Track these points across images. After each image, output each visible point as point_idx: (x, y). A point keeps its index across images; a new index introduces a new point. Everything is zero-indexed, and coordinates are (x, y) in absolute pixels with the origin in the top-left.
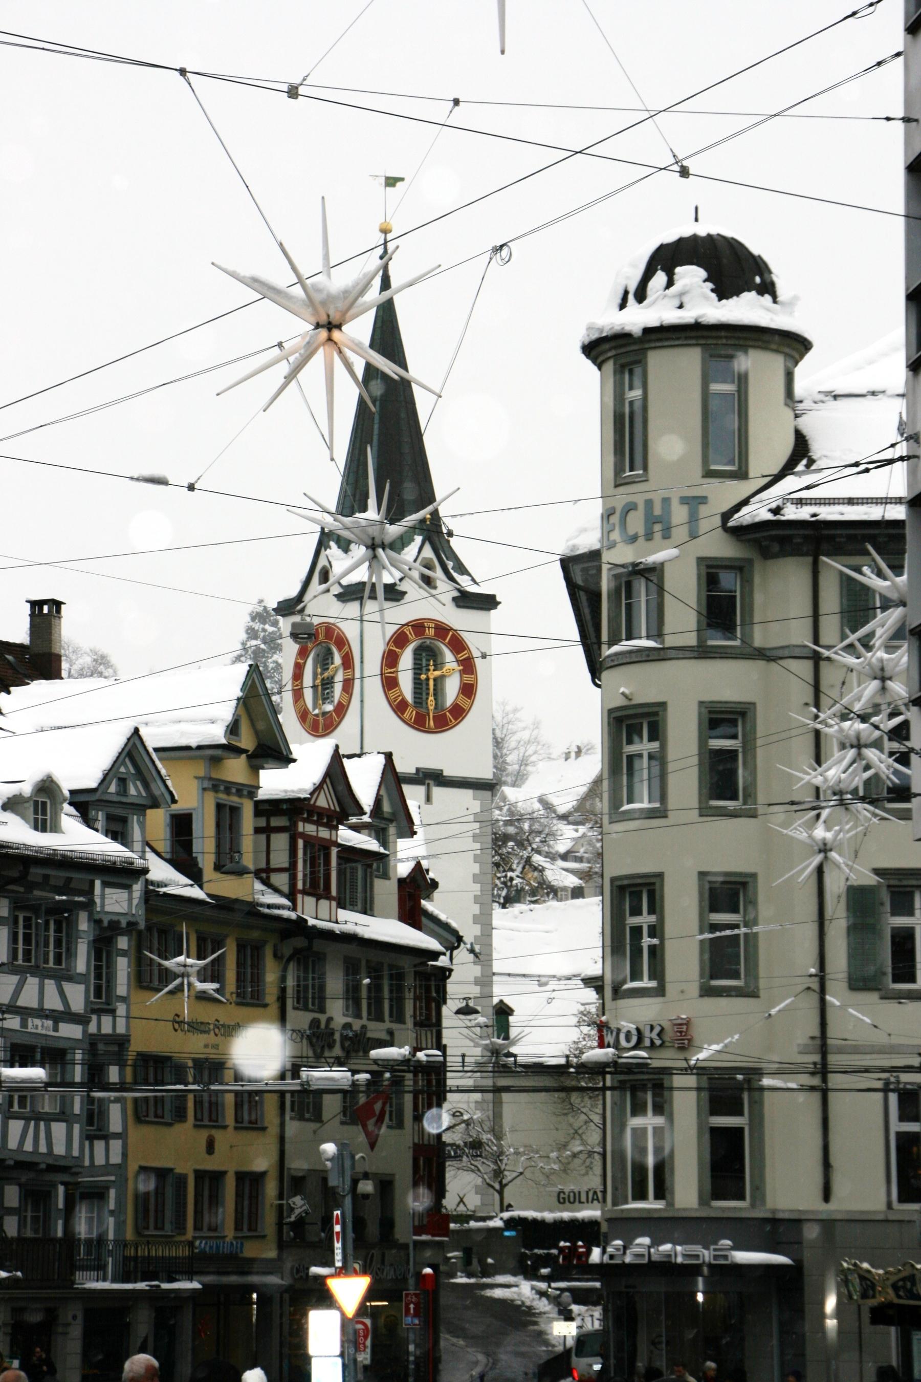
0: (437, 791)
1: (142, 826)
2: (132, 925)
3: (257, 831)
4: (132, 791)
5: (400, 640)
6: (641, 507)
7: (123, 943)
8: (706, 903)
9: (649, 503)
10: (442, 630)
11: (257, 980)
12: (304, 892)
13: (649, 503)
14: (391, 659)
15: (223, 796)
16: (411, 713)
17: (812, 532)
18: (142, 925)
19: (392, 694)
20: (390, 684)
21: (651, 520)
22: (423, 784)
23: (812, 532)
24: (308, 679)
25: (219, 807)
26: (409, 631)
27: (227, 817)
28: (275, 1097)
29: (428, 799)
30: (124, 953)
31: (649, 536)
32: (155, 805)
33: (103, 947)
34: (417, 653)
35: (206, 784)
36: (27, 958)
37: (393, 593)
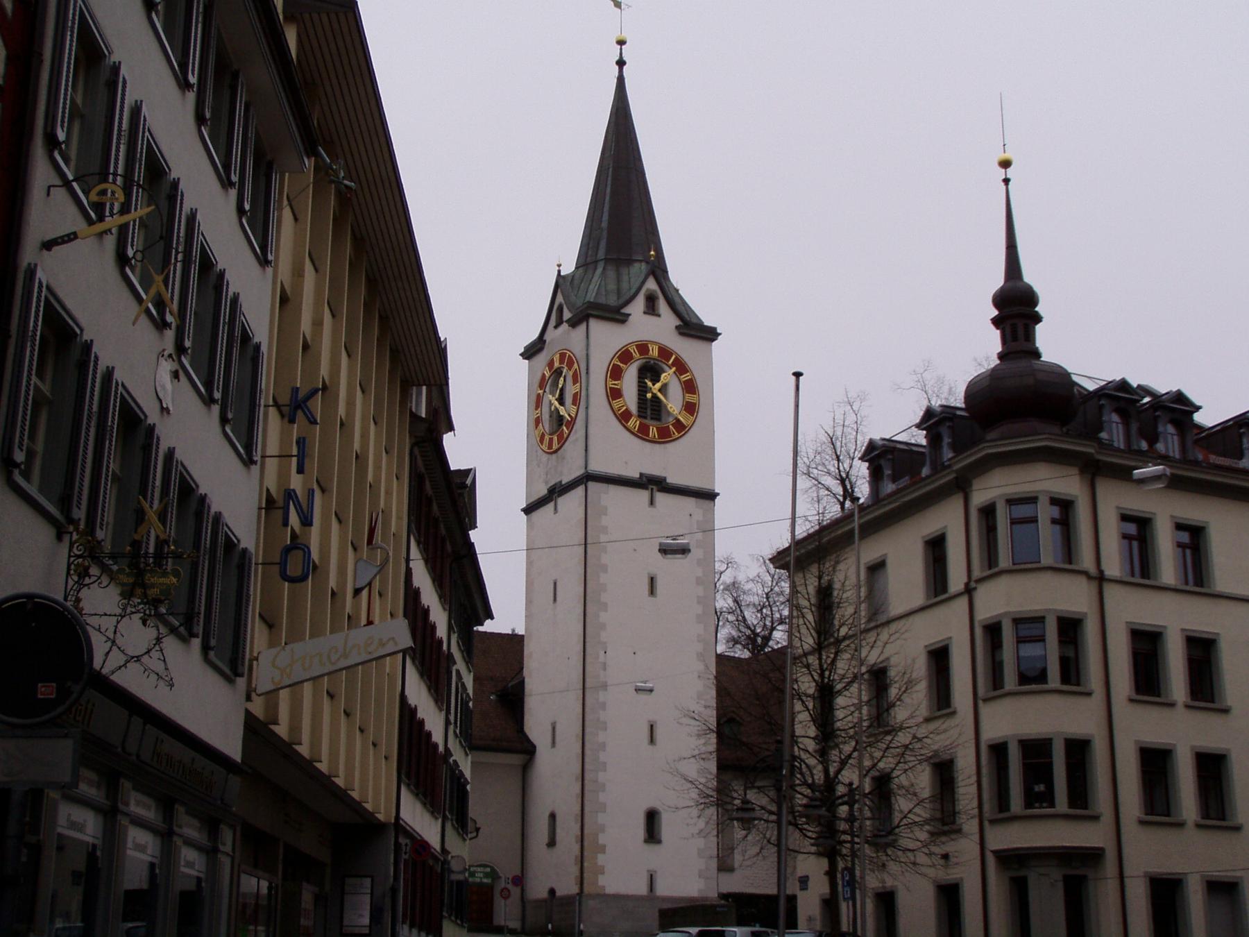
0: (660, 497)
5: (625, 356)
8: (1018, 616)
10: (665, 353)
14: (616, 373)
17: (470, 691)
20: (615, 394)
22: (646, 488)
23: (470, 691)
26: (611, 383)
28: (1022, 646)
29: (652, 503)
37: (616, 315)
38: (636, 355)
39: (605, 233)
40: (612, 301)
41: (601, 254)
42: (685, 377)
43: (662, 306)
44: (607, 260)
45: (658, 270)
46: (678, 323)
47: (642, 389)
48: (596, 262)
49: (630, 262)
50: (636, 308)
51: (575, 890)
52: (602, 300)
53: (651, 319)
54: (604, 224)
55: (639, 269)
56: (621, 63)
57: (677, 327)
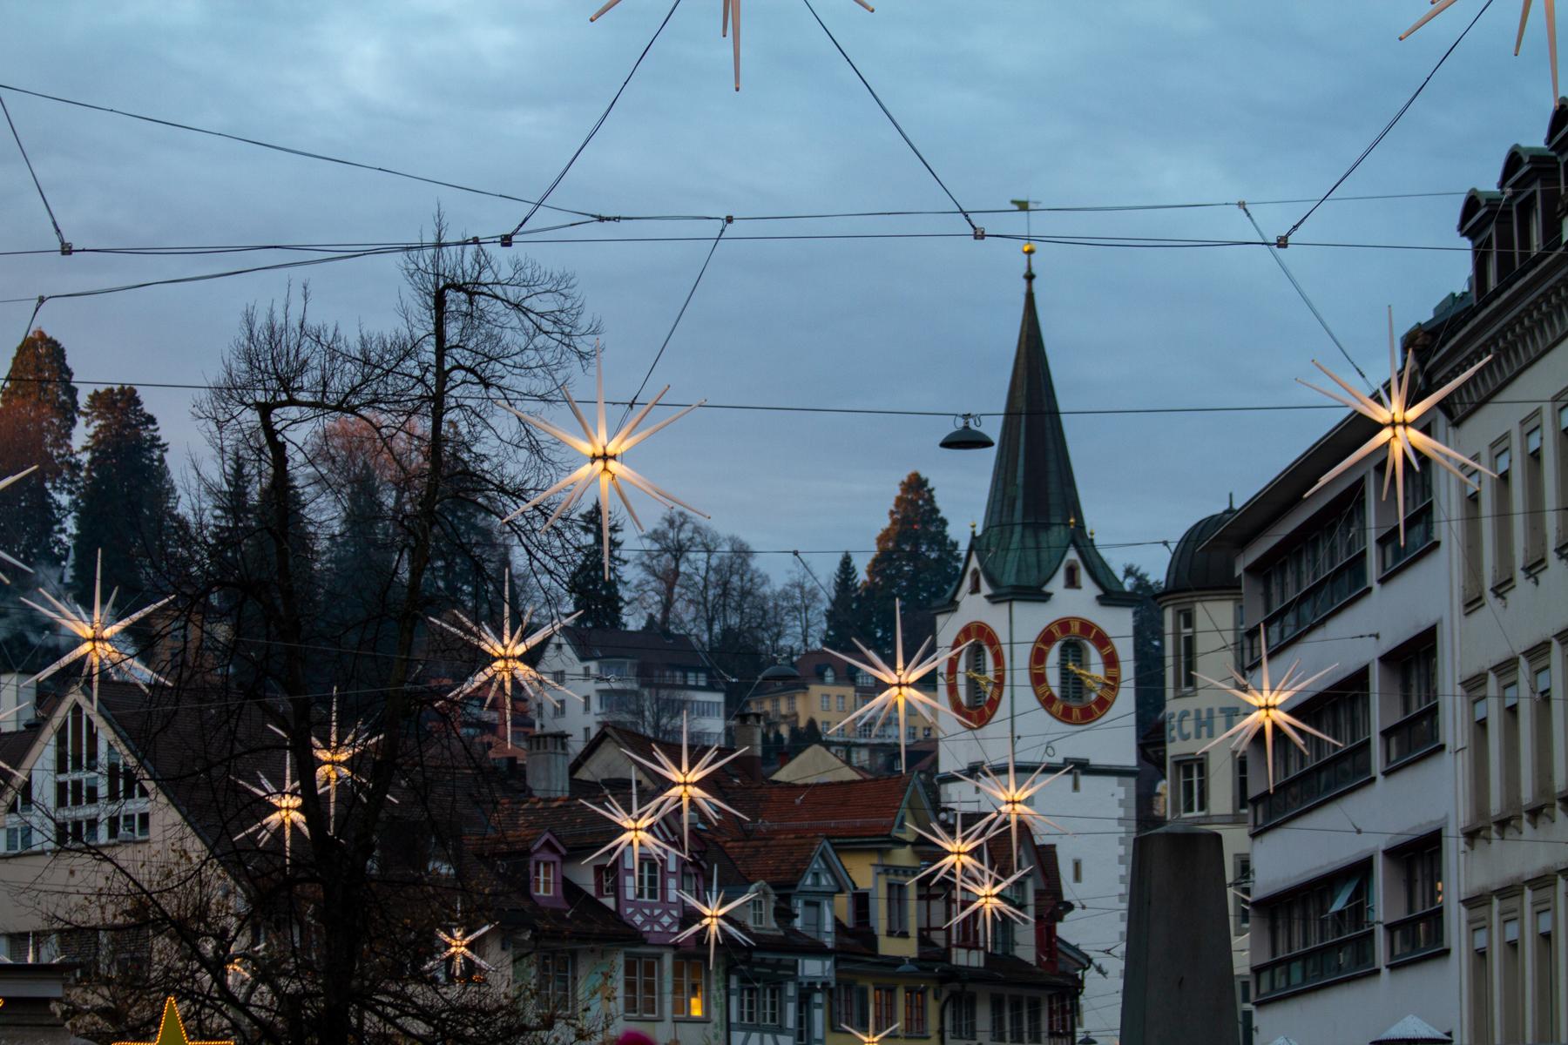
0: (1085, 780)
1: (831, 906)
2: (825, 985)
3: (920, 897)
4: (824, 882)
5: (1047, 638)
6: (1193, 716)
7: (818, 998)
9: (1198, 712)
10: (1087, 627)
11: (922, 1020)
12: (958, 946)
13: (1198, 712)
14: (1039, 657)
15: (892, 877)
16: (1058, 707)
18: (833, 984)
19: (1041, 690)
20: (1038, 679)
21: (1199, 723)
24: (961, 680)
25: (890, 886)
26: (1056, 630)
27: (896, 893)
29: (1076, 787)
30: (820, 1006)
31: (1198, 736)
32: (841, 891)
33: (804, 1001)
34: (1063, 651)
35: (880, 869)
36: (751, 1019)
37: (1038, 595)
38: (1058, 634)
39: (1020, 493)
40: (1031, 579)
41: (1018, 517)
42: (1107, 651)
43: (1084, 577)
44: (1025, 525)
45: (1080, 538)
46: (1100, 592)
47: (1065, 674)
48: (1013, 525)
49: (1047, 526)
50: (1057, 585)
51: (1132, 781)
52: (1024, 582)
53: (1072, 592)
54: (1020, 480)
55: (1056, 535)
56: (1030, 277)
57: (1098, 598)
